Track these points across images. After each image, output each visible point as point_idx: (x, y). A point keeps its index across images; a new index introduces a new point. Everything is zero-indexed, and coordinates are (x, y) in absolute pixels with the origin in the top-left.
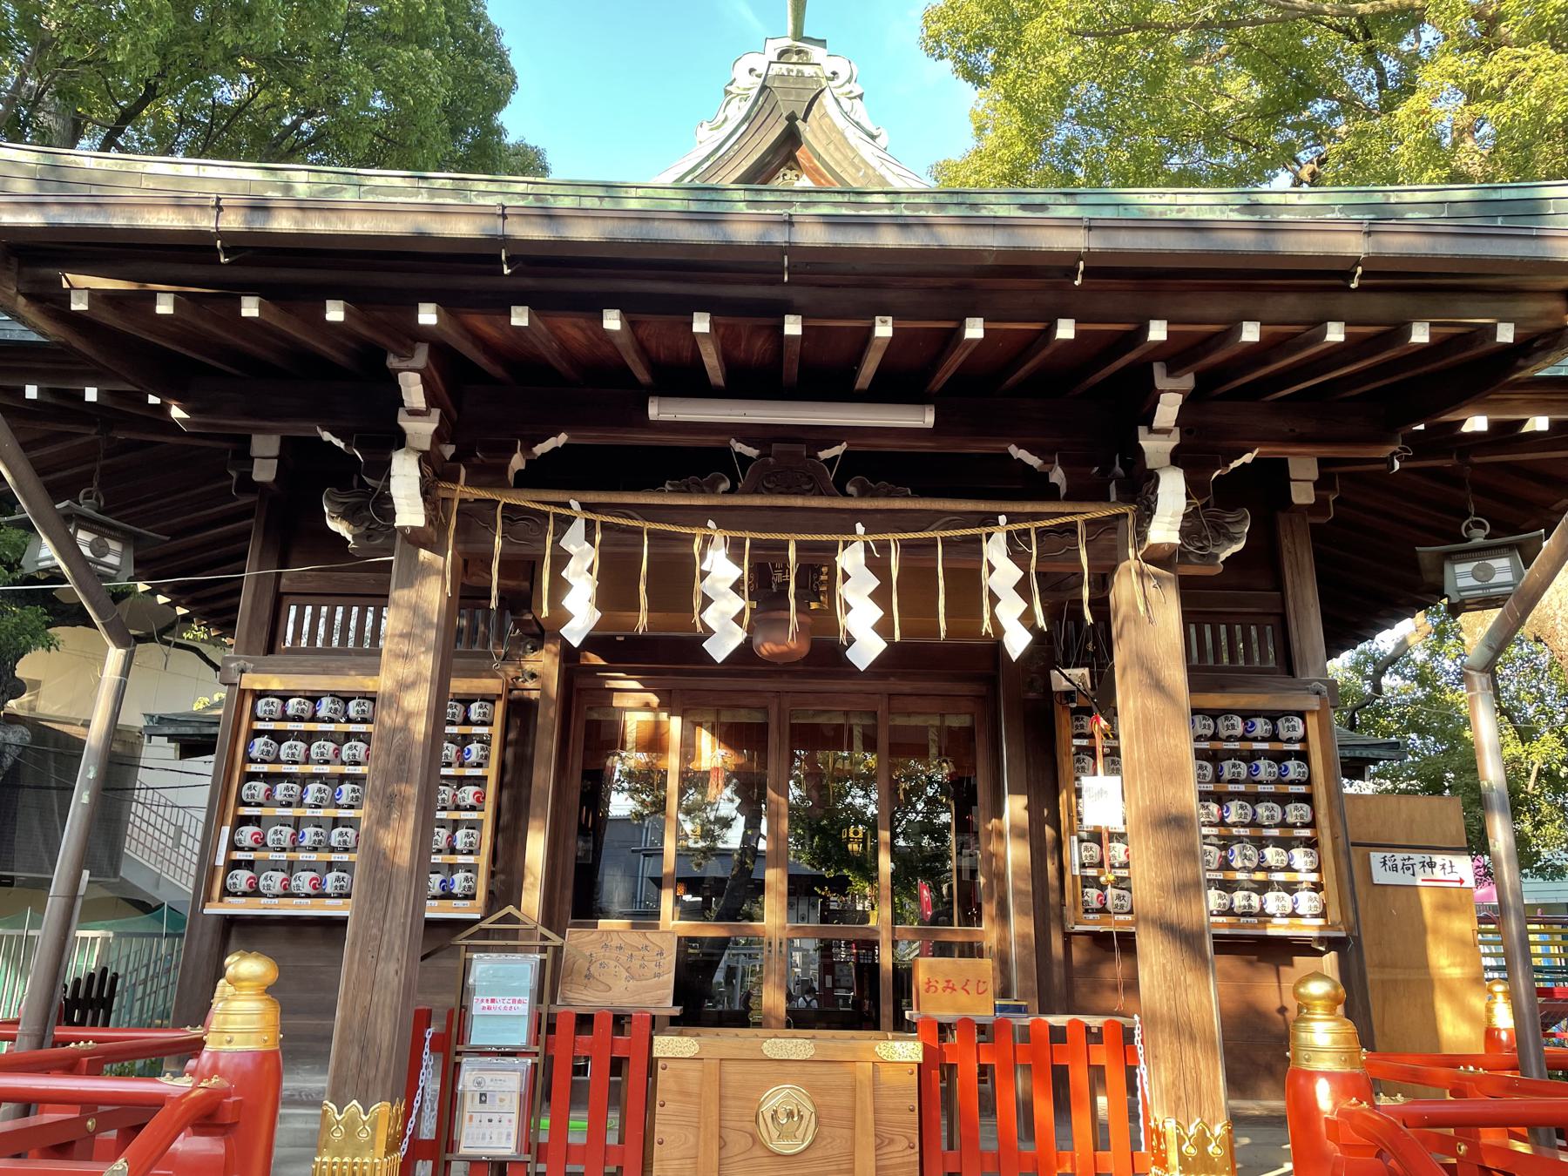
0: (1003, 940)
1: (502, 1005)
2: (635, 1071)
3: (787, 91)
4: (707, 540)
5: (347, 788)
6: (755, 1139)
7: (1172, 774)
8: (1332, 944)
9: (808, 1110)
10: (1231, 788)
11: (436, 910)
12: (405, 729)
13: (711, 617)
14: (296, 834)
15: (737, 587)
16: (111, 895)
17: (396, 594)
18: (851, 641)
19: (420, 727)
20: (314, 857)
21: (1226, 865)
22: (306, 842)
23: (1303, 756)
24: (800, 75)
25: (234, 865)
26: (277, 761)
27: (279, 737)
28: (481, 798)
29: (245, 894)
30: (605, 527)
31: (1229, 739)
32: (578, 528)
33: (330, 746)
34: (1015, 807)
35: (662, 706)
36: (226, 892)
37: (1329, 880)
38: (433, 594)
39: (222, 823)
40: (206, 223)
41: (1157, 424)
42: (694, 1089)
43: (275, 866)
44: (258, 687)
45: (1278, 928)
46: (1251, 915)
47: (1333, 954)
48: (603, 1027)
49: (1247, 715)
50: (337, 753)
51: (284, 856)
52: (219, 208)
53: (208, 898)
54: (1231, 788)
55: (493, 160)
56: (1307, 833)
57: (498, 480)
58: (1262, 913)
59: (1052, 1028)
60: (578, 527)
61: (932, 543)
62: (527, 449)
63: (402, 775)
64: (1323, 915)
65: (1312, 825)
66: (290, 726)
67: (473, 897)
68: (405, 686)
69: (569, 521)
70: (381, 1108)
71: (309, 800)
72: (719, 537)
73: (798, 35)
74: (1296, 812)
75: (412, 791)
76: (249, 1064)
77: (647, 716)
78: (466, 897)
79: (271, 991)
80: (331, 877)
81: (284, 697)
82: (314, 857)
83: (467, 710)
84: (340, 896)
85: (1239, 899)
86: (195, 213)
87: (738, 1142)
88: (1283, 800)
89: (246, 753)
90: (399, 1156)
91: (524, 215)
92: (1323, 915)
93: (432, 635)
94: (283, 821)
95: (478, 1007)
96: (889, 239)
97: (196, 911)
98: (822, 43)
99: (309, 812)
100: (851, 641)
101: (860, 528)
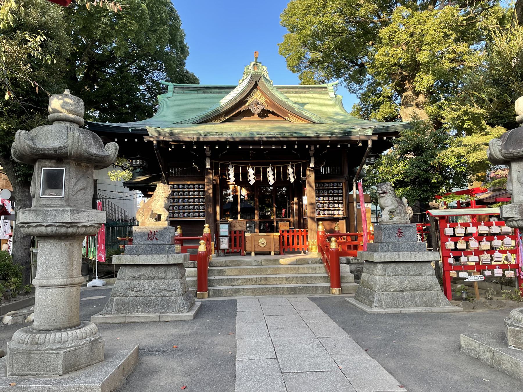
0: (293, 220)
1: (224, 230)
2: (243, 238)
4: (249, 167)
6: (259, 245)
7: (312, 198)
8: (344, 218)
12: (209, 195)
13: (250, 178)
15: (254, 174)
17: (206, 176)
19: (212, 195)
21: (328, 207)
23: (342, 189)
24: (257, 74)
30: (235, 166)
31: (331, 187)
32: (230, 166)
34: (295, 200)
35: (236, 184)
37: (345, 210)
40: (192, 140)
45: (336, 216)
47: (345, 220)
48: (238, 233)
49: (184, 185)
55: (176, 41)
56: (342, 201)
58: (334, 214)
64: (343, 214)
65: (342, 200)
66: (175, 190)
68: (209, 189)
69: (229, 165)
71: (180, 202)
72: (250, 167)
73: (256, 62)
74: (340, 198)
77: (233, 186)
85: (330, 212)
87: (256, 246)
88: (338, 196)
92: (343, 214)
94: (177, 205)
96: (274, 139)
98: (260, 63)
100: (270, 181)
101: (270, 165)
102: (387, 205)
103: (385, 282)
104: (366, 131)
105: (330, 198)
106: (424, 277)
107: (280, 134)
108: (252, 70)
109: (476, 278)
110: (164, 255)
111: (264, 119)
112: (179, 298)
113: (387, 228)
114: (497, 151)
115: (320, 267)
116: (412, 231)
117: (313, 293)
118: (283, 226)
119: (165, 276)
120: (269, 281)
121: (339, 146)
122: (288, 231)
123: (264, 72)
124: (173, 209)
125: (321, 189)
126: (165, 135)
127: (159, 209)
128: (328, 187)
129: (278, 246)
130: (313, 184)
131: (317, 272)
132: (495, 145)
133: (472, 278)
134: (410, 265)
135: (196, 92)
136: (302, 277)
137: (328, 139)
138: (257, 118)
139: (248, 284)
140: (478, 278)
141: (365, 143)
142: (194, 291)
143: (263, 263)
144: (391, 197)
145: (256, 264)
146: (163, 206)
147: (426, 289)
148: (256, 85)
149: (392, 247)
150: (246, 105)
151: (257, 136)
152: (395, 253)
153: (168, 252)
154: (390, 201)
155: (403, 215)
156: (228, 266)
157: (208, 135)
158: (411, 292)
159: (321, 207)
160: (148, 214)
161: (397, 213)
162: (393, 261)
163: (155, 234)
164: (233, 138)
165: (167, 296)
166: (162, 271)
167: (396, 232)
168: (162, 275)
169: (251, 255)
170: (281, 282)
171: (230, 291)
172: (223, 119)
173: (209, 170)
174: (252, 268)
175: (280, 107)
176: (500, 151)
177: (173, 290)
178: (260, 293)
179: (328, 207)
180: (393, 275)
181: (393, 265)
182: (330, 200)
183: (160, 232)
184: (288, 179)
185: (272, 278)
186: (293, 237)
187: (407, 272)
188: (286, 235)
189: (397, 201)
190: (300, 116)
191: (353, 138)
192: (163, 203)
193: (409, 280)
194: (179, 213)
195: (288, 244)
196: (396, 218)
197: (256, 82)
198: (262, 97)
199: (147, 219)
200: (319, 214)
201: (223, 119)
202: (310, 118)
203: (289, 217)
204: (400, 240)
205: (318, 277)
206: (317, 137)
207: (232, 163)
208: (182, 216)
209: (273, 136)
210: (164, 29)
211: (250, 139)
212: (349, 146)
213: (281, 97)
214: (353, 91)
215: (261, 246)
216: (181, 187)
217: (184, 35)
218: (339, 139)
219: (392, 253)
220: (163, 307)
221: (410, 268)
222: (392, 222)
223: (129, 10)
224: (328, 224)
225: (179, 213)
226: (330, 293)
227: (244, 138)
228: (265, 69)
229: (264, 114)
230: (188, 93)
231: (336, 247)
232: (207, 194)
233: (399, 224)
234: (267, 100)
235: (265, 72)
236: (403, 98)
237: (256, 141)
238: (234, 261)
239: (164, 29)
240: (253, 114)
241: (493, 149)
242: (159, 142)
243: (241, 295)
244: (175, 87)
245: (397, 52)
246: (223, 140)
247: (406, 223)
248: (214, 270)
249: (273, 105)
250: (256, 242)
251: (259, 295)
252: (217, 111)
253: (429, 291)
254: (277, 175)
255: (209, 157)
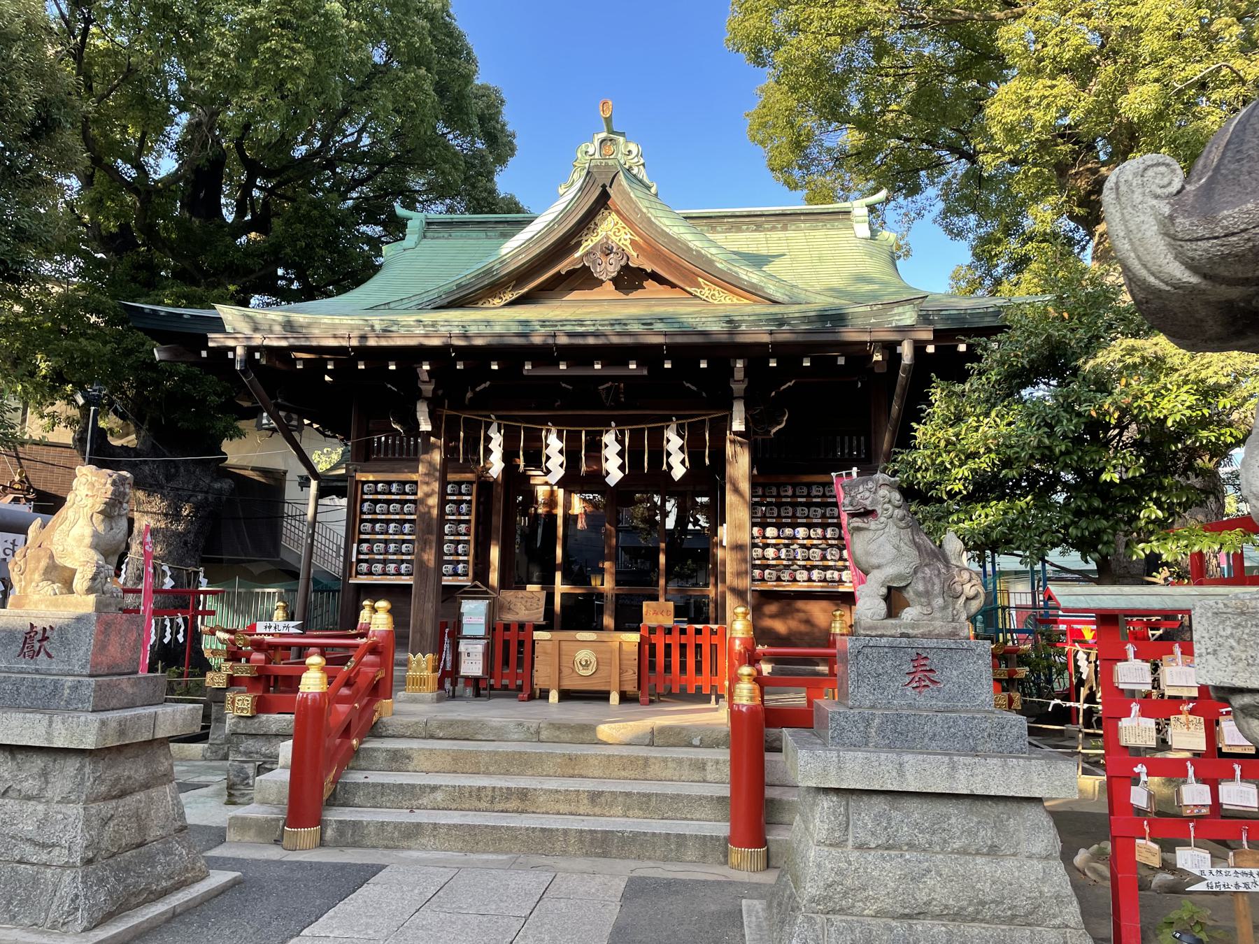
2: (528, 646)
3: (600, 173)
4: (548, 431)
5: (407, 525)
6: (573, 670)
9: (593, 660)
10: (830, 521)
11: (447, 581)
12: (429, 512)
14: (386, 547)
15: (561, 452)
16: (273, 568)
17: (422, 457)
18: (608, 474)
19: (435, 512)
20: (395, 557)
21: (824, 558)
22: (391, 551)
24: (607, 164)
25: (359, 561)
26: (375, 513)
27: (375, 502)
28: (468, 530)
29: (366, 574)
31: (788, 497)
32: (495, 426)
33: (398, 506)
36: (358, 573)
38: (437, 457)
39: (353, 542)
40: (344, 343)
41: (736, 378)
42: (549, 651)
43: (378, 561)
44: (363, 479)
46: (834, 582)
48: (514, 629)
50: (402, 509)
51: (381, 557)
52: (350, 338)
53: (350, 576)
54: (830, 521)
55: (467, 114)
57: (463, 408)
58: (841, 581)
59: (696, 629)
60: (495, 426)
61: (643, 430)
62: (473, 389)
63: (430, 533)
66: (380, 497)
67: (467, 575)
68: (428, 495)
69: (492, 423)
70: (429, 656)
71: (391, 531)
75: (433, 538)
76: (384, 634)
78: (464, 575)
79: (389, 611)
80: (403, 566)
81: (376, 483)
82: (395, 557)
83: (460, 488)
84: (408, 575)
85: (829, 574)
86: (341, 340)
87: (566, 671)
89: (361, 510)
90: (438, 674)
91: (458, 337)
93: (437, 474)
94: (380, 541)
95: (465, 620)
96: (591, 341)
97: (345, 582)
98: (622, 134)
99: (391, 537)
100: (608, 474)
101: (613, 424)
102: (874, 561)
103: (840, 872)
104: (896, 311)
105: (829, 533)
106: (1010, 863)
107: (612, 325)
108: (597, 156)
109: (1241, 880)
110: (39, 716)
111: (631, 296)
112: (68, 876)
113: (867, 650)
114: (1151, 230)
115: (717, 762)
116: (972, 667)
117: (665, 859)
118: (655, 613)
119: (41, 790)
120: (534, 802)
121: (807, 363)
122: (669, 631)
123: (632, 161)
124: (371, 551)
125: (801, 504)
126: (271, 331)
127: (73, 554)
128: (824, 496)
129: (631, 676)
130: (745, 486)
131: (709, 777)
132: (1137, 197)
133: (1223, 880)
134: (950, 808)
135: (482, 235)
136: (644, 795)
137: (766, 338)
138: (610, 292)
139: (467, 806)
140: (1250, 880)
141: (890, 348)
142: (278, 820)
143: (544, 734)
144: (894, 530)
145: (522, 736)
146: (88, 540)
147: (1014, 916)
148: (603, 201)
149: (881, 730)
150: (577, 255)
151: (543, 330)
152: (883, 756)
153: (68, 703)
154: (889, 547)
155: (939, 602)
156: (432, 737)
157: (394, 328)
158: (951, 925)
159: (799, 557)
160: (36, 568)
161: (918, 594)
162: (877, 788)
163: (45, 638)
164: (465, 336)
165: (33, 864)
166: (35, 770)
167: (908, 667)
168: (30, 785)
169: (547, 698)
170: (573, 808)
171: (389, 829)
172: (509, 297)
173: (432, 439)
174: (496, 753)
175: (675, 257)
176: (1167, 227)
177: (53, 845)
178: (487, 844)
179: (824, 558)
180: (878, 846)
181: (880, 804)
182: (828, 536)
183: (62, 631)
184: (665, 467)
185: (546, 791)
186: (683, 647)
187: (935, 839)
188: (660, 641)
189: (918, 546)
190: (730, 284)
191: (850, 335)
192: (88, 531)
193: (945, 871)
194: (385, 562)
195: (668, 667)
196: (909, 614)
197: (604, 186)
198: (622, 231)
199: (33, 584)
200: (795, 580)
201: (509, 297)
202: (762, 289)
203: (707, 585)
204: (921, 700)
205: (701, 798)
206: (730, 333)
207: (498, 418)
208: (393, 571)
209: (592, 329)
210: (417, 76)
211: (517, 341)
212: (841, 361)
213: (675, 229)
214: (958, 234)
215: (583, 672)
216: (394, 488)
217: (502, 101)
218: (800, 338)
219: (873, 757)
220: (9, 903)
221: (953, 820)
222: (895, 627)
223: (288, 17)
224: (825, 611)
225: (385, 562)
226: (726, 863)
227: (501, 336)
228: (635, 152)
229: (629, 279)
230: (462, 237)
231: (752, 698)
232: (422, 509)
233: (923, 636)
234: (637, 238)
235: (636, 160)
236: (1096, 239)
237: (537, 345)
238: (452, 723)
239: (417, 76)
240: (600, 283)
241: (1125, 221)
242: (250, 350)
243: (424, 848)
244: (428, 224)
245: (1055, 91)
246: (436, 342)
247: (953, 635)
248: (374, 750)
249: (656, 255)
250: (564, 658)
251: (484, 852)
252: (488, 272)
253: (1029, 925)
254: (632, 456)
255: (426, 399)
